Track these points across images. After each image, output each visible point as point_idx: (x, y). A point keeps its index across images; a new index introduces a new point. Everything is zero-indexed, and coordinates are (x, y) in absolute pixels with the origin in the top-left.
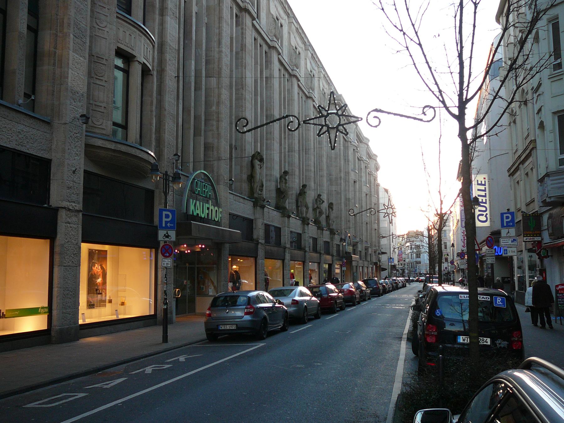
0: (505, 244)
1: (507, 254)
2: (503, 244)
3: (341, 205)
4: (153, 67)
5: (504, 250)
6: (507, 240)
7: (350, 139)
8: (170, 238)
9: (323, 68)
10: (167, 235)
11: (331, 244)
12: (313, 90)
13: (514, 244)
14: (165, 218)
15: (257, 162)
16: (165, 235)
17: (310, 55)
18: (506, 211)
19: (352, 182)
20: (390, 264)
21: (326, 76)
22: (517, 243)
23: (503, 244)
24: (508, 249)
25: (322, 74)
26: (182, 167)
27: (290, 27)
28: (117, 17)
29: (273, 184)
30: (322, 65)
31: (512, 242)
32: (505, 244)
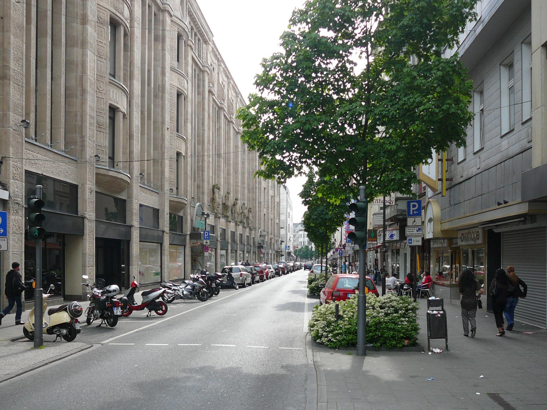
0: (410, 233)
1: (411, 243)
2: (408, 233)
4: (127, 113)
5: (409, 239)
7: (167, 6)
11: (184, 218)
12: (224, 101)
15: (216, 190)
17: (239, 100)
19: (262, 189)
20: (287, 251)
21: (215, 50)
23: (408, 233)
25: (210, 46)
26: (51, 143)
27: (219, 69)
28: (110, 82)
29: (221, 200)
32: (410, 233)
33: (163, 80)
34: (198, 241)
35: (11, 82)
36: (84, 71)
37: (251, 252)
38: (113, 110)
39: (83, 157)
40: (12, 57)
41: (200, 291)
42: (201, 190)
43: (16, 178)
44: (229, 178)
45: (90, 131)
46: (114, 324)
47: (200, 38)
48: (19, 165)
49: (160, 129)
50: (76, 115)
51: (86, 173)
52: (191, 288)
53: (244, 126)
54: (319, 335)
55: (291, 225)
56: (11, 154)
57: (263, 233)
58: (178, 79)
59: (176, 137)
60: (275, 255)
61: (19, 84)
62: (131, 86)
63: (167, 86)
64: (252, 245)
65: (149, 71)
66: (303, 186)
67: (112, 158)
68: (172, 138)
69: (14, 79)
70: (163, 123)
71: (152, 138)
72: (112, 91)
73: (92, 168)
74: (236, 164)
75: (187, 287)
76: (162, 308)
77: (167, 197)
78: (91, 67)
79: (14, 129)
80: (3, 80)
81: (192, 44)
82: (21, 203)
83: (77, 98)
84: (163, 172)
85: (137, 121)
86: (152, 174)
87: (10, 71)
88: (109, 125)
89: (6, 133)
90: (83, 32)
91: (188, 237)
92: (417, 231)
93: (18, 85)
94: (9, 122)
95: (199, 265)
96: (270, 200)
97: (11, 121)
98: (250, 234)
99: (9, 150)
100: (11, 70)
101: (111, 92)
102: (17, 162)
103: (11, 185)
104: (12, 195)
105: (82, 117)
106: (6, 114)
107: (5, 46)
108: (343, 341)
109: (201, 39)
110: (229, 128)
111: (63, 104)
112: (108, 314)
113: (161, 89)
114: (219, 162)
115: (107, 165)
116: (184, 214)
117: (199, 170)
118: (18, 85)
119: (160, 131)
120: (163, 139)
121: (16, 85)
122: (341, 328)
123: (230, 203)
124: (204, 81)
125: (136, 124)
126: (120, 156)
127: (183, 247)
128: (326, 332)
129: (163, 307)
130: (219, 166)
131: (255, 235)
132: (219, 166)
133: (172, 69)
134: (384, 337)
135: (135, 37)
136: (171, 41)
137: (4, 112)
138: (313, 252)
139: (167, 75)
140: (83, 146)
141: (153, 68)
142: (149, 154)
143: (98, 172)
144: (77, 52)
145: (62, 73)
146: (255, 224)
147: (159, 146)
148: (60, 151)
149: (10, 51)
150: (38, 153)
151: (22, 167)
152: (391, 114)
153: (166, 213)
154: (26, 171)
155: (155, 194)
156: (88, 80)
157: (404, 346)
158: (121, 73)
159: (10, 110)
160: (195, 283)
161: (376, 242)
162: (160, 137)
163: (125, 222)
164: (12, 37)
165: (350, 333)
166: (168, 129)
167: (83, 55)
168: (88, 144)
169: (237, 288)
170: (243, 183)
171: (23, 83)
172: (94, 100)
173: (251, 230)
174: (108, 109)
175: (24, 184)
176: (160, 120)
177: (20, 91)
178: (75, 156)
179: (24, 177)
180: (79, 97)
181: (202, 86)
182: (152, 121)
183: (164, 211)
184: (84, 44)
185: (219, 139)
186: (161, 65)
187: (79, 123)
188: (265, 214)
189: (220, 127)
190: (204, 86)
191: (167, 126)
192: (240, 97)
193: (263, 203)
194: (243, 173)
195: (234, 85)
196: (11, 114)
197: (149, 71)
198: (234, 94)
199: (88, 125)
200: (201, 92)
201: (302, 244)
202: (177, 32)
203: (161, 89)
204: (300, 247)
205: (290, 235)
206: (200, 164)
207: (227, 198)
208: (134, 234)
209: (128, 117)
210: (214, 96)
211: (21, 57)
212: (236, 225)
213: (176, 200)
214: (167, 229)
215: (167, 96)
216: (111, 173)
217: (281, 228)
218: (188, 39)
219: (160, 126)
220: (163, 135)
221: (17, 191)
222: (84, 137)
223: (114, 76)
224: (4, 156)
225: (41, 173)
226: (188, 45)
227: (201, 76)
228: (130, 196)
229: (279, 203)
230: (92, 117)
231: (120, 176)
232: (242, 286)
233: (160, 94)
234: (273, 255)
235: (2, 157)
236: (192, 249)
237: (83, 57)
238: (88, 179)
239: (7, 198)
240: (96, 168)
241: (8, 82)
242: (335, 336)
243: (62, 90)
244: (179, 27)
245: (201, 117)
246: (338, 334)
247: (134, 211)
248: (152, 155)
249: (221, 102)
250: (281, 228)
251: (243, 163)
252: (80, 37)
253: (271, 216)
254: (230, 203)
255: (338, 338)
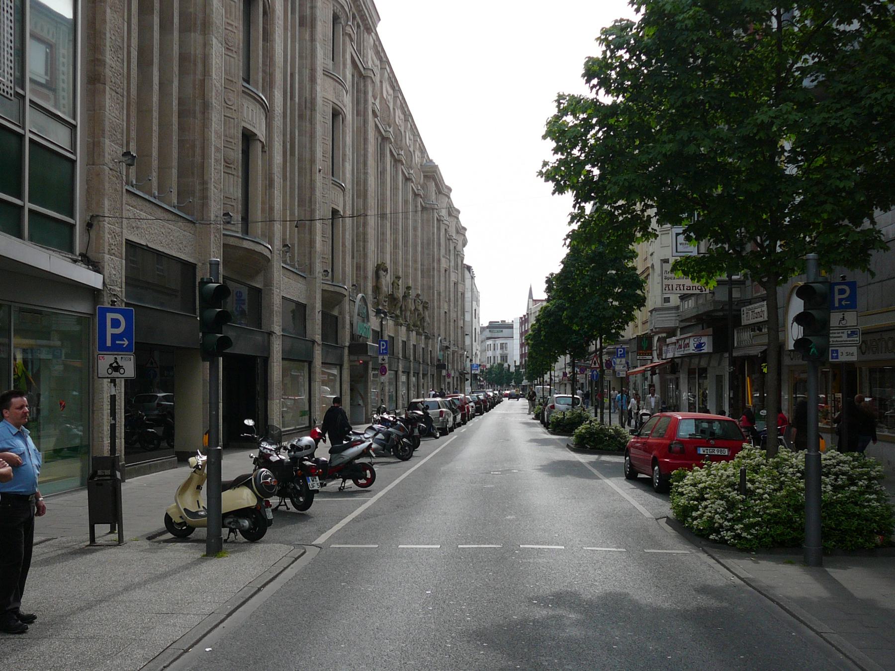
1: (837, 357)
3: (433, 302)
6: (839, 333)
8: (122, 371)
9: (419, 135)
10: (115, 365)
11: (340, 320)
13: (854, 341)
14: (112, 327)
15: (382, 273)
16: (111, 365)
18: (839, 280)
19: (443, 270)
22: (858, 339)
24: (840, 350)
27: (382, 75)
28: (243, 92)
30: (418, 133)
31: (848, 337)
33: (313, 90)
34: (360, 357)
35: (107, 88)
36: (206, 72)
37: (427, 374)
38: (248, 137)
39: (205, 217)
40: (108, 44)
41: (398, 443)
42: (362, 273)
43: (113, 251)
44: (396, 253)
45: (215, 172)
46: (308, 504)
47: (360, 22)
48: (118, 230)
49: (308, 171)
50: (193, 146)
51: (210, 243)
52: (383, 438)
53: (556, 151)
54: (716, 525)
55: (478, 330)
56: (106, 211)
57: (446, 344)
58: (334, 89)
59: (331, 185)
60: (459, 378)
61: (118, 90)
62: (271, 98)
63: (319, 101)
64: (429, 363)
65: (292, 75)
66: (562, 262)
67: (245, 219)
68: (325, 186)
69: (111, 82)
70: (313, 161)
71: (296, 187)
72: (245, 106)
73: (218, 236)
74: (405, 230)
75: (377, 437)
76: (366, 475)
77: (320, 283)
78: (217, 66)
79: (111, 167)
80: (94, 84)
81: (351, 33)
82: (119, 294)
83: (195, 117)
84: (312, 243)
85: (278, 159)
86: (296, 245)
87: (105, 68)
88: (242, 164)
89: (98, 175)
90: (205, 6)
91: (346, 351)
92: (849, 336)
93: (117, 93)
94: (104, 156)
95: (359, 397)
96: (452, 290)
97: (106, 155)
98: (427, 344)
99: (103, 204)
100: (107, 66)
101: (245, 108)
102: (115, 225)
103: (106, 264)
104: (107, 281)
105: (203, 148)
106: (99, 142)
107: (97, 27)
108: (765, 537)
109: (361, 24)
110: (396, 171)
111: (175, 127)
112: (295, 488)
113: (308, 105)
114: (383, 226)
115: (240, 230)
116: (340, 313)
117: (361, 238)
118: (117, 93)
119: (308, 175)
120: (312, 189)
121: (114, 94)
122: (756, 514)
123: (400, 294)
124: (366, 93)
125: (278, 161)
126: (257, 213)
127: (306, 364)
128: (729, 521)
129: (368, 472)
130: (383, 234)
131: (433, 346)
132: (383, 234)
133: (326, 73)
134: (840, 530)
135: (277, 18)
136: (323, 27)
137: (96, 140)
138: (512, 373)
139: (319, 81)
140: (205, 198)
141: (297, 69)
142: (292, 214)
143: (226, 242)
144: (196, 38)
145: (174, 75)
146: (433, 329)
147: (306, 199)
148: (171, 206)
149: (105, 34)
150: (141, 210)
151: (122, 233)
152: (847, 123)
153: (317, 310)
154: (129, 243)
155: (301, 279)
156: (214, 88)
157: (877, 546)
158: (258, 76)
159: (106, 136)
160: (390, 429)
161: (650, 357)
162: (308, 185)
163: (260, 326)
164: (108, 10)
165: (777, 523)
166: (320, 171)
167: (205, 45)
168: (212, 195)
169: (438, 436)
170: (415, 261)
171: (123, 89)
172: (221, 121)
173: (427, 338)
174: (240, 136)
175: (124, 261)
176: (308, 156)
177: (119, 104)
178: (192, 215)
179: (124, 250)
180: (199, 115)
181: (362, 101)
182: (297, 159)
183: (314, 308)
184: (206, 26)
185: (383, 189)
186: (308, 66)
187: (198, 159)
188: (445, 312)
189: (384, 168)
190: (366, 101)
191: (319, 166)
192: (410, 120)
193: (443, 295)
194: (415, 246)
195: (402, 102)
196: (107, 142)
197: (292, 75)
198: (402, 117)
199: (213, 163)
200: (362, 110)
201: (492, 361)
202: (332, 12)
203: (308, 105)
204: (488, 366)
205: (477, 347)
206: (361, 229)
207: (396, 284)
208: (275, 345)
209: (266, 148)
210: (376, 119)
211: (121, 46)
212: (409, 329)
213: (331, 289)
214: (318, 338)
215: (319, 117)
216: (246, 245)
217: (466, 335)
218: (347, 24)
219: (308, 166)
220: (312, 182)
221: (115, 275)
222: (207, 184)
223: (248, 82)
224: (95, 214)
225: (145, 244)
226: (346, 33)
227: (362, 85)
228: (268, 283)
229: (463, 294)
230: (218, 150)
231: (259, 248)
232: (445, 432)
233: (308, 113)
234: (455, 379)
235: (92, 216)
236: (352, 369)
237: (205, 48)
238: (212, 253)
239: (99, 286)
240: (224, 235)
241: (102, 86)
242: (747, 528)
243: (174, 104)
244: (336, 4)
245: (362, 152)
246: (753, 525)
247: (275, 308)
248: (296, 215)
249: (386, 128)
250: (466, 335)
251: (415, 229)
252: (200, 16)
253: (453, 315)
254: (400, 294)
255: (754, 531)
